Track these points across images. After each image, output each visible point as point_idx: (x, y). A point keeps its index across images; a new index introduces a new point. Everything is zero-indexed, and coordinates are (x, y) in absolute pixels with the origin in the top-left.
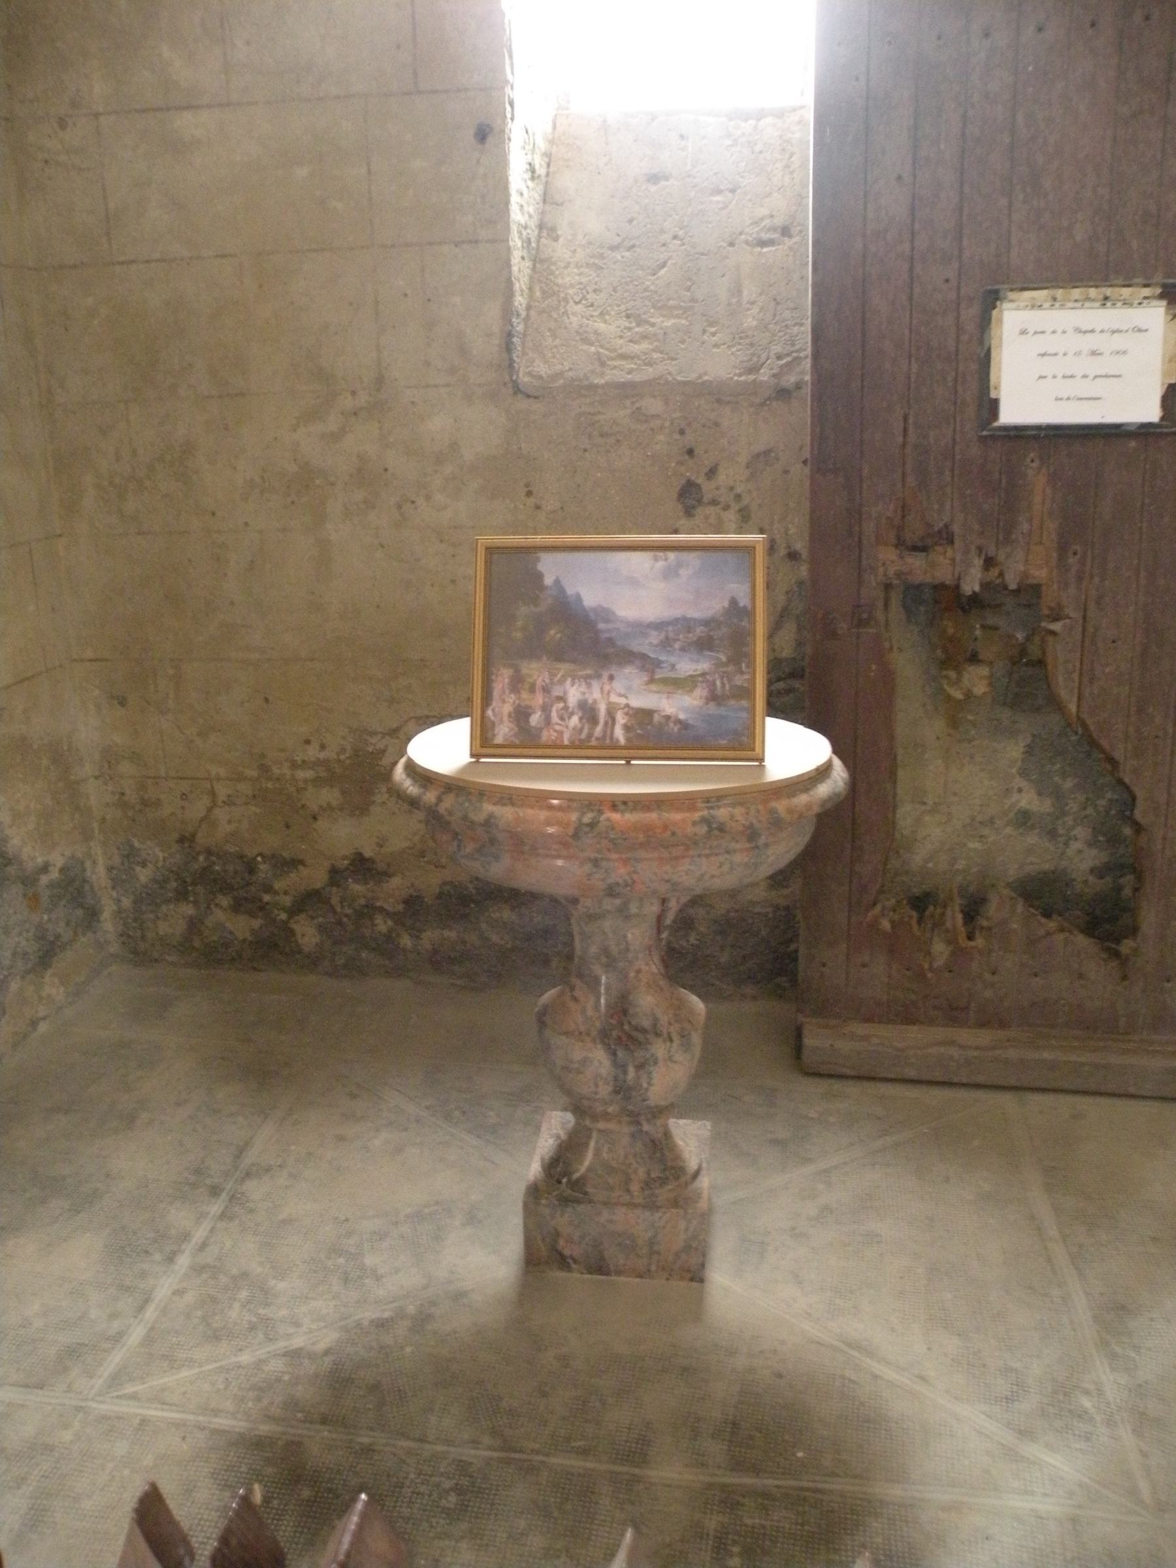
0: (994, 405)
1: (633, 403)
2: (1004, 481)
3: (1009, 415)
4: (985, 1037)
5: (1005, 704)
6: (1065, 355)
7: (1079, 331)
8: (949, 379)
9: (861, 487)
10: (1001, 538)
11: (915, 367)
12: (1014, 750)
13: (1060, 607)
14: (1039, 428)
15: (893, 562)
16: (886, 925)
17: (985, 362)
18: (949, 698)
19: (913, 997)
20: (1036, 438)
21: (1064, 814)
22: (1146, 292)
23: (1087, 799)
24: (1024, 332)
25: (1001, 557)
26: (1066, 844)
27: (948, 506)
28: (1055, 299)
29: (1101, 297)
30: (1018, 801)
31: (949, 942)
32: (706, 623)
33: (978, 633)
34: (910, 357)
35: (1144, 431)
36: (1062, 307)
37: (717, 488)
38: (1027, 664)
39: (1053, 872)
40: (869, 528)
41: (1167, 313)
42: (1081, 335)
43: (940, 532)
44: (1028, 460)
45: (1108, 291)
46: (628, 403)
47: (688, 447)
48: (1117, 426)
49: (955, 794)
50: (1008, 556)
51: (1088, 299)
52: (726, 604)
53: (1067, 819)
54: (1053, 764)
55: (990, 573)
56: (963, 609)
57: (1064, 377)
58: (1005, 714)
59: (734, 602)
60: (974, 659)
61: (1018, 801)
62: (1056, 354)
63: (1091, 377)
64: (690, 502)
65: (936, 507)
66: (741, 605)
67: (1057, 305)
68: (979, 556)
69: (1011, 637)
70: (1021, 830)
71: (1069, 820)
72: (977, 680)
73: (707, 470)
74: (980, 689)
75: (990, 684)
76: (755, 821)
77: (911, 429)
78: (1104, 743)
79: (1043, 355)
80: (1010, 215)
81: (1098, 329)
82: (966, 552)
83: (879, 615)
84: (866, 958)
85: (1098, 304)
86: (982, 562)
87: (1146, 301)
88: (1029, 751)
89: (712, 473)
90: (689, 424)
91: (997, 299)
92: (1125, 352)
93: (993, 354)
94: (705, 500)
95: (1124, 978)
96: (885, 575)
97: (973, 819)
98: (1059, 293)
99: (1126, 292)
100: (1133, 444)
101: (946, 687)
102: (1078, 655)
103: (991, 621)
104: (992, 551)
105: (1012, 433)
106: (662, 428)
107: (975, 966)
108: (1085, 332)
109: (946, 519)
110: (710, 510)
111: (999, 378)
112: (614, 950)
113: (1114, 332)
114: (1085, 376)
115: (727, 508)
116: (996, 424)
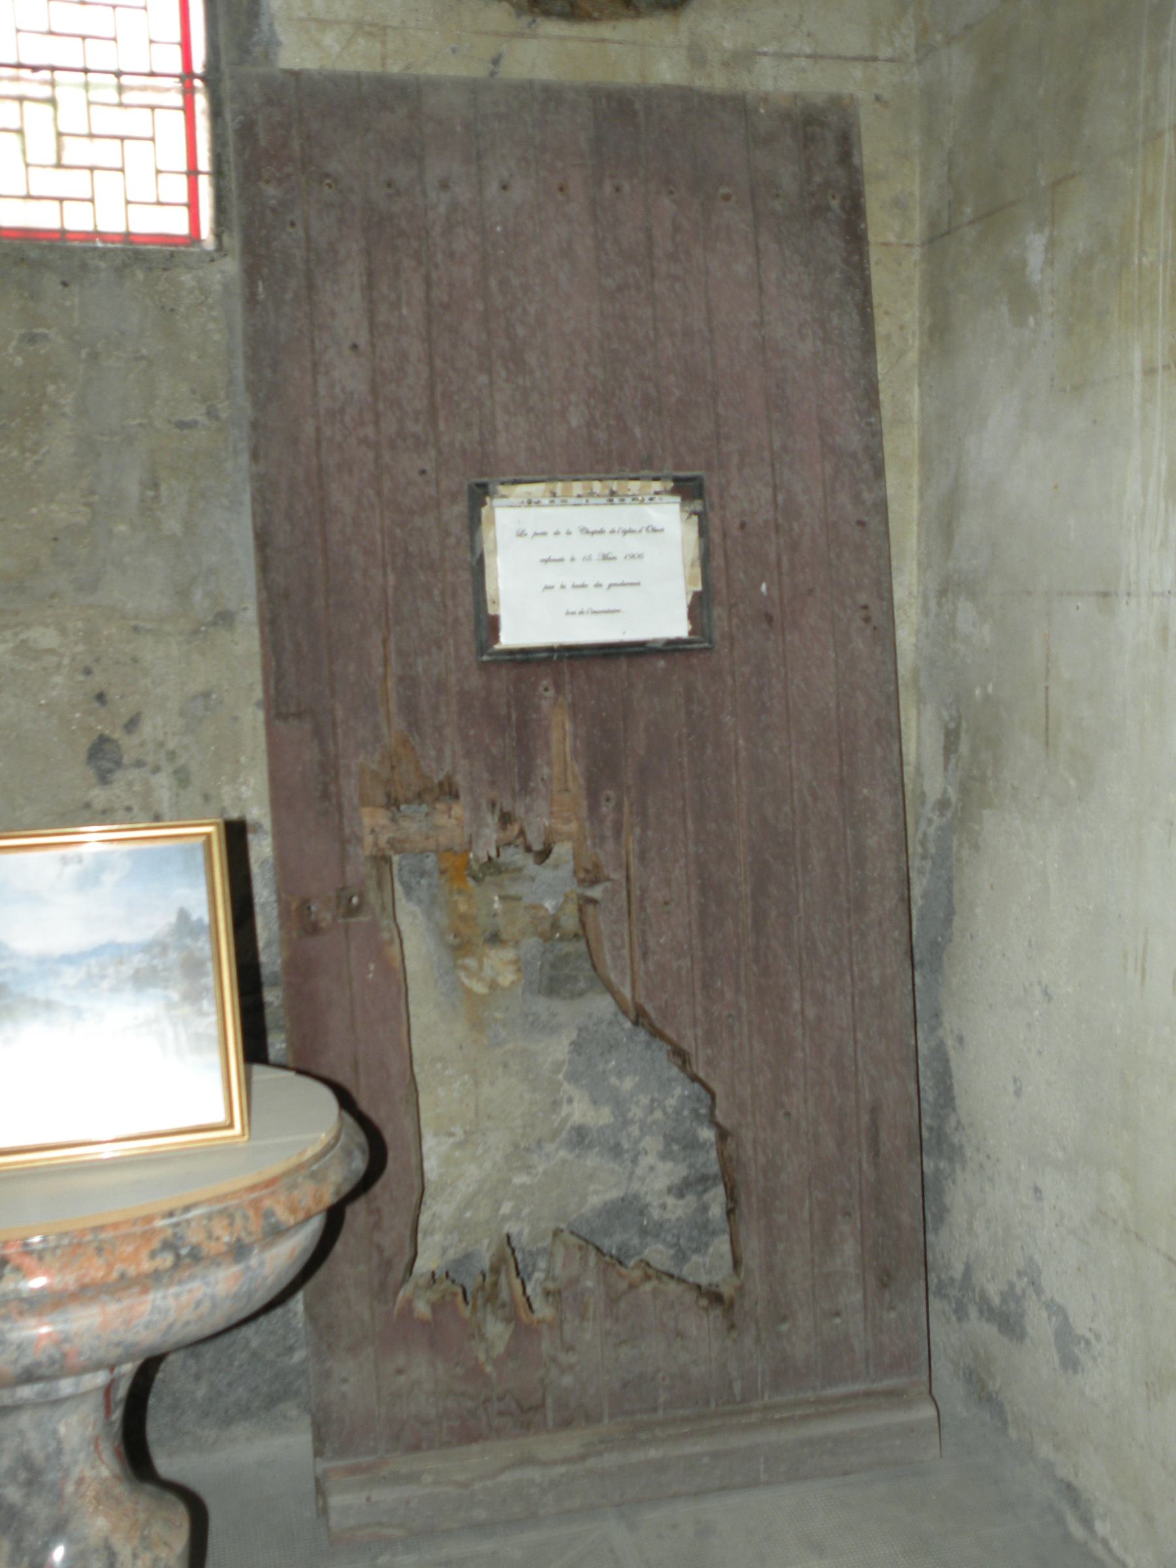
0: (494, 625)
1: (16, 634)
2: (514, 716)
3: (510, 637)
4: (569, 1443)
5: (539, 992)
6: (573, 559)
7: (585, 531)
8: (436, 592)
9: (335, 734)
10: (517, 787)
11: (391, 578)
12: (557, 1050)
13: (597, 866)
14: (550, 650)
15: (383, 827)
16: (422, 1308)
17: (478, 570)
18: (469, 992)
19: (469, 1404)
20: (547, 661)
21: (626, 1123)
22: (657, 486)
23: (653, 1100)
24: (521, 534)
25: (520, 811)
26: (635, 1161)
27: (448, 752)
28: (554, 495)
29: (607, 492)
30: (569, 1116)
31: (507, 1320)
32: (147, 948)
33: (497, 906)
34: (384, 565)
35: (671, 648)
36: (564, 503)
37: (142, 745)
38: (561, 939)
39: (623, 1200)
40: (350, 787)
41: (682, 510)
42: (589, 536)
43: (441, 784)
44: (541, 689)
45: (615, 485)
46: (8, 634)
47: (97, 691)
48: (641, 644)
49: (489, 1117)
50: (528, 810)
51: (592, 494)
52: (173, 919)
53: (630, 1129)
54: (607, 1062)
55: (508, 833)
56: (475, 878)
57: (574, 586)
58: (541, 1005)
59: (183, 915)
60: (495, 939)
61: (569, 1116)
62: (562, 560)
63: (606, 585)
64: (107, 765)
65: (433, 753)
66: (194, 917)
67: (557, 501)
68: (493, 812)
69: (537, 907)
70: (577, 1151)
71: (635, 1131)
72: (499, 965)
73: (125, 720)
74: (507, 978)
75: (519, 970)
76: (243, 1235)
77: (393, 657)
78: (670, 1033)
79: (546, 561)
80: (492, 396)
81: (608, 529)
82: (476, 808)
83: (372, 897)
84: (401, 1360)
85: (604, 500)
86: (496, 819)
87: (657, 497)
88: (577, 1047)
89: (132, 724)
90: (97, 660)
91: (487, 493)
92: (640, 556)
93: (488, 561)
94: (126, 760)
95: (732, 1327)
96: (376, 844)
97: (516, 1147)
98: (559, 487)
99: (634, 486)
100: (661, 663)
101: (466, 981)
102: (626, 925)
103: (513, 890)
104: (507, 804)
105: (519, 657)
106: (59, 666)
107: (545, 1345)
108: (593, 533)
109: (447, 768)
110: (134, 774)
111: (497, 589)
112: (39, 1456)
113: (625, 532)
114: (598, 585)
115: (157, 769)
116: (497, 647)
